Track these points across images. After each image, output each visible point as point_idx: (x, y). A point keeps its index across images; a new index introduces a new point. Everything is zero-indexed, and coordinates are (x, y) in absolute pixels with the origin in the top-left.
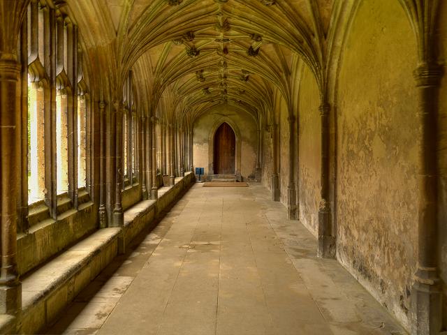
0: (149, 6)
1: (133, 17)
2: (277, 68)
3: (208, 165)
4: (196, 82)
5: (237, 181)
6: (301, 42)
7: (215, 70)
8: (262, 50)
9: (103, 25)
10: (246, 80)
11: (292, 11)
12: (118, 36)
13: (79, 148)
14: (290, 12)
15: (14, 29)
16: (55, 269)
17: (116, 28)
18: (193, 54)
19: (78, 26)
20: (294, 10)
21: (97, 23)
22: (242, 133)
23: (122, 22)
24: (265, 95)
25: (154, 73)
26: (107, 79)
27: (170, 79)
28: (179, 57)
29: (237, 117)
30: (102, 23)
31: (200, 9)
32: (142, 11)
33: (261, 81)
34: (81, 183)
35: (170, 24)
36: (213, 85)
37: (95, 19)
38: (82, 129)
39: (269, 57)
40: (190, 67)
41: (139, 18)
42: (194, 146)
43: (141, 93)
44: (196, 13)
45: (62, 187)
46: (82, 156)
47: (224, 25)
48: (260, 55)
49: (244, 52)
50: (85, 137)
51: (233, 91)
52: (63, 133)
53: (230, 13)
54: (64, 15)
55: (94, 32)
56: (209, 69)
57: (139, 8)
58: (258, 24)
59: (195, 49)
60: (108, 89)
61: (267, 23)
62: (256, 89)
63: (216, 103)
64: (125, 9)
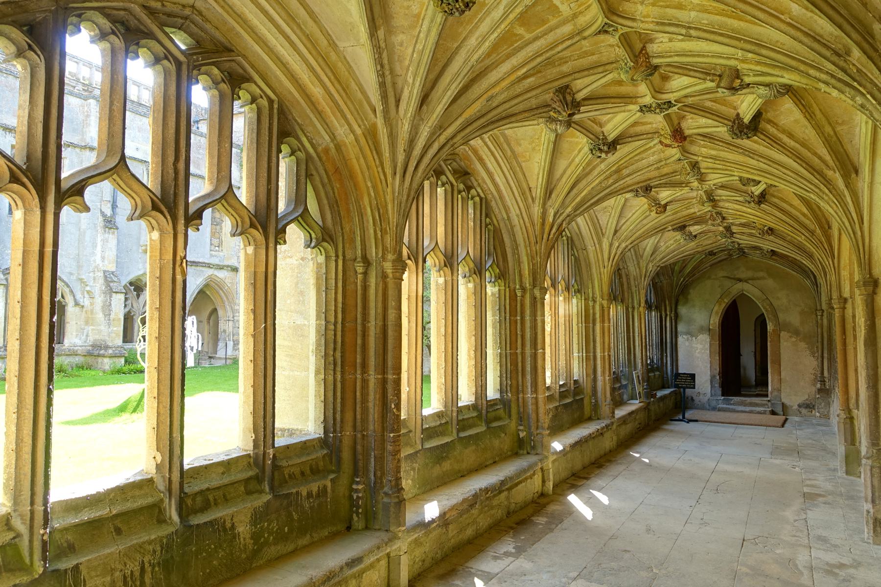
3: (708, 378)
5: (773, 413)
6: (840, 55)
8: (769, 122)
10: (759, 203)
16: (862, 363)
22: (781, 316)
24: (812, 233)
33: (796, 202)
34: (492, 393)
36: (699, 220)
39: (791, 136)
42: (681, 340)
49: (722, 131)
53: (634, 20)
55: (320, 114)
58: (734, 37)
61: (735, 23)
62: (788, 220)
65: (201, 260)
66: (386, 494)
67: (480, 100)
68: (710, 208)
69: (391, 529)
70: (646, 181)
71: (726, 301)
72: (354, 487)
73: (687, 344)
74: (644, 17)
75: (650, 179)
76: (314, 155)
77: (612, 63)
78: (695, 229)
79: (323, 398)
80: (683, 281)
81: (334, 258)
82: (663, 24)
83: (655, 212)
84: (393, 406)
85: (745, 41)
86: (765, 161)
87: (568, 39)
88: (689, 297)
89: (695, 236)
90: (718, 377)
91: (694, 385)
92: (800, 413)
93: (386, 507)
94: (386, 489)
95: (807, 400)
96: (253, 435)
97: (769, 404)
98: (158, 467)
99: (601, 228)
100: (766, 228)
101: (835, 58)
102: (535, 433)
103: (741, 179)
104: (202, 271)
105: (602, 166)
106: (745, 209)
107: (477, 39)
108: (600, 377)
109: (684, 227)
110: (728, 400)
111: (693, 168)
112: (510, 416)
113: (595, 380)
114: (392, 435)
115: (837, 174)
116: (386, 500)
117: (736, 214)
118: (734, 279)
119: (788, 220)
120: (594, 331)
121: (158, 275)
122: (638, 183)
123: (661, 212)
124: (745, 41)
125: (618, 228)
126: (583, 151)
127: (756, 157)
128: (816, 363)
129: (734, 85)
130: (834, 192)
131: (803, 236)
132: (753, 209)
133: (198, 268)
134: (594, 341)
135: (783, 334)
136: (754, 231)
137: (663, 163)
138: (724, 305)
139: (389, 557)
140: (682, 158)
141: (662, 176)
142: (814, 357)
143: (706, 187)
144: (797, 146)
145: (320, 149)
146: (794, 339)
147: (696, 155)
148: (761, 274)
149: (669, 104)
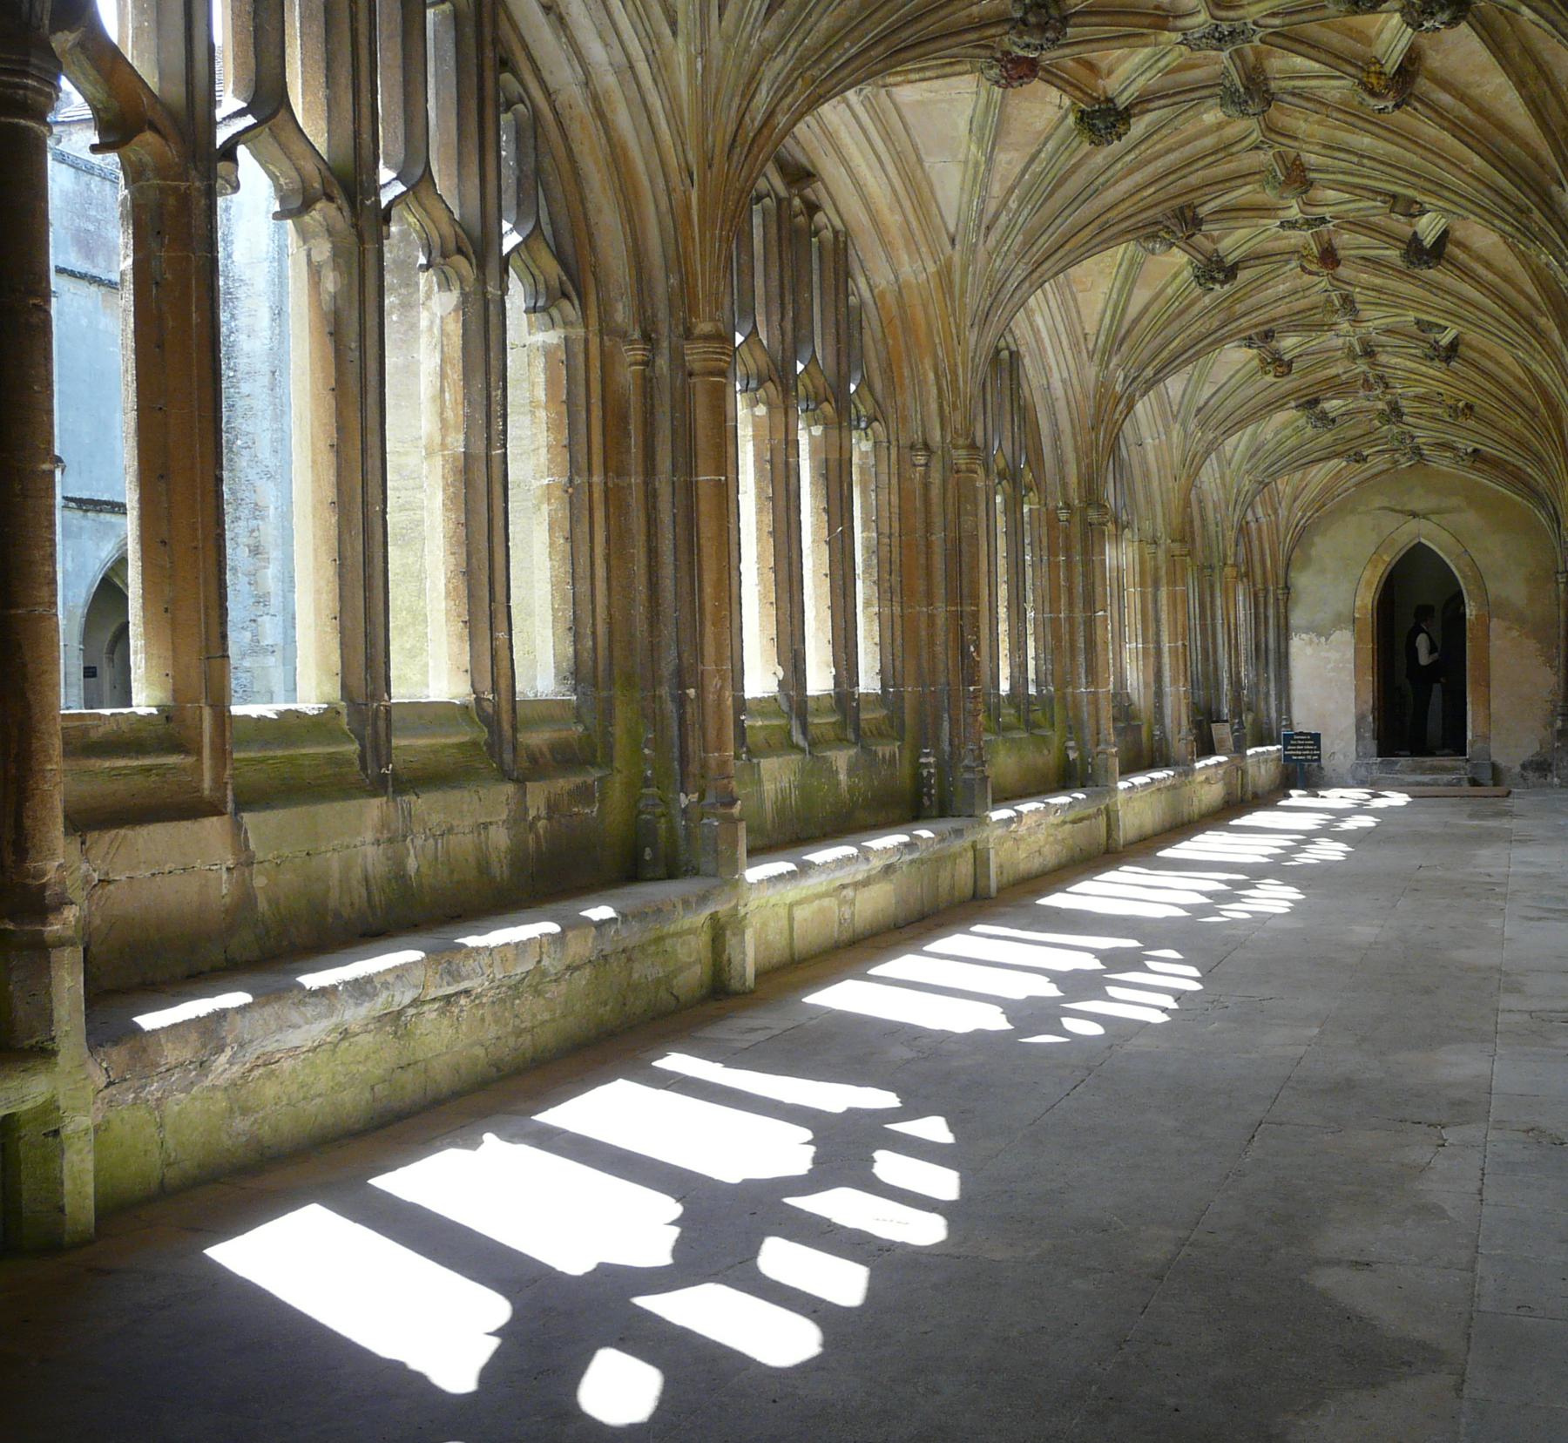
0: (1039, 151)
1: (997, 189)
2: (1523, 303)
5: (1474, 782)
7: (1321, 327)
8: (1460, 244)
9: (914, 224)
10: (1447, 360)
11: (1471, 115)
12: (958, 247)
13: (859, 584)
14: (1465, 120)
15: (718, 269)
17: (952, 229)
18: (1214, 280)
19: (847, 234)
20: (1480, 110)
21: (898, 218)
23: (964, 207)
24: (1533, 412)
25: (1091, 356)
26: (931, 375)
27: (1149, 372)
28: (1169, 291)
29: (1470, 519)
30: (912, 218)
31: (1197, 137)
32: (1018, 170)
34: (868, 682)
35: (1110, 195)
36: (1339, 387)
37: (891, 210)
38: (865, 528)
39: (1488, 265)
40: (1216, 324)
41: (1011, 190)
43: (1055, 424)
44: (1187, 150)
45: (819, 680)
46: (867, 604)
47: (1288, 176)
48: (1453, 262)
49: (1393, 254)
50: (873, 550)
51: (1427, 410)
53: (1296, 138)
54: (812, 208)
55: (886, 245)
56: (1294, 328)
57: (1009, 163)
59: (1221, 260)
60: (934, 407)
62: (1494, 389)
63: (1378, 463)
64: (971, 171)
65: (105, 498)
66: (968, 769)
67: (1091, 227)
68: (1365, 368)
69: (977, 813)
70: (1268, 322)
71: (1387, 559)
72: (923, 760)
73: (1309, 651)
74: (1308, 136)
75: (1274, 320)
76: (871, 302)
77: (1255, 173)
78: (1333, 405)
79: (877, 640)
80: (1302, 518)
81: (885, 444)
82: (1330, 147)
83: (1272, 374)
84: (972, 649)
85: (1425, 179)
86: (1455, 300)
87: (1212, 154)
88: (1313, 552)
89: (1333, 421)
90: (1371, 718)
91: (1319, 755)
93: (969, 785)
94: (966, 762)
95: (1538, 754)
96: (833, 670)
98: (780, 683)
99: (1170, 403)
100: (1461, 405)
101: (1517, 215)
102: (1094, 751)
103: (1418, 322)
104: (112, 526)
105: (1207, 300)
106: (1424, 369)
107: (1104, 158)
108: (1168, 689)
109: (1316, 401)
111: (1344, 302)
112: (1053, 725)
113: (1159, 694)
114: (971, 688)
115: (1552, 324)
116: (967, 776)
117: (1409, 379)
118: (1401, 512)
119: (1494, 389)
120: (1156, 601)
121: (768, 458)
122: (1256, 326)
123: (1283, 375)
124: (1425, 179)
126: (1180, 278)
127: (1440, 293)
128: (1555, 679)
129: (1412, 211)
130: (1549, 350)
131: (1519, 420)
132: (1439, 369)
133: (102, 515)
134: (1157, 620)
135: (1495, 623)
136: (1439, 411)
137: (1298, 296)
138: (1381, 569)
139: (975, 851)
140: (1330, 288)
141: (1294, 314)
142: (1551, 667)
143: (1362, 330)
144: (1498, 280)
145: (876, 291)
146: (1515, 634)
147: (1349, 284)
148: (1454, 501)
149: (1323, 220)
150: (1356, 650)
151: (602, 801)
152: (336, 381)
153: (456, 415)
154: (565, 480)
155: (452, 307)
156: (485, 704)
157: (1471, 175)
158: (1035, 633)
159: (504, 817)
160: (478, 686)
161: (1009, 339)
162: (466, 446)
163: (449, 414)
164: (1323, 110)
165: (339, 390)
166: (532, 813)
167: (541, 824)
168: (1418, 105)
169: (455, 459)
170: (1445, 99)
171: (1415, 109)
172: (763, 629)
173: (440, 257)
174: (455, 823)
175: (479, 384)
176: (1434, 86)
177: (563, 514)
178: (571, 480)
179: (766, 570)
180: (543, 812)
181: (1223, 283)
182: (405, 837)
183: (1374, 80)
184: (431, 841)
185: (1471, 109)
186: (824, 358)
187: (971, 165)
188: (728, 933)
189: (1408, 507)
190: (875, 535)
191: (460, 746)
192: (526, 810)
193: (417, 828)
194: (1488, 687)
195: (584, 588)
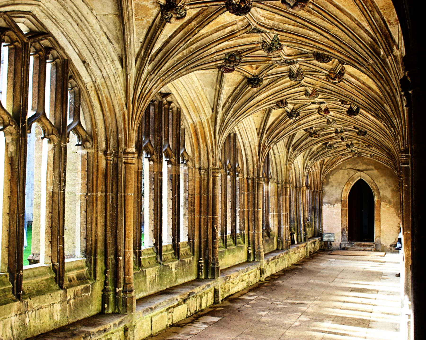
0: (237, 87)
4: (310, 138)
18: (293, 116)
19: (180, 109)
28: (281, 118)
32: (231, 91)
41: (229, 97)
44: (282, 86)
52: (168, 196)
72: (200, 261)
73: (328, 209)
79: (187, 225)
92: (391, 250)
97: (374, 245)
98: (154, 244)
110: (351, 244)
124: (350, 99)
125: (215, 67)
135: (382, 203)
137: (319, 119)
146: (388, 206)
148: (371, 167)
150: (342, 210)
151: (92, 291)
152: (11, 177)
153: (50, 180)
154: (85, 194)
155: (51, 149)
156: (55, 266)
157: (362, 100)
158: (240, 215)
159: (59, 301)
160: (53, 261)
161: (233, 130)
162: (53, 190)
163: (49, 180)
164: (319, 80)
165: (11, 180)
166: (68, 298)
167: (72, 301)
168: (345, 82)
169: (50, 193)
170: (353, 80)
171: (344, 83)
172: (150, 228)
173: (47, 134)
174: (42, 305)
175: (57, 171)
176: (350, 77)
177: (84, 204)
178: (87, 194)
179: (151, 210)
180: (72, 297)
181: (295, 117)
182: (25, 312)
183: (332, 75)
184: (34, 312)
185: (362, 83)
186: (172, 145)
187: (217, 91)
188: (129, 330)
189: (357, 168)
190: (187, 194)
191: (47, 280)
192: (66, 297)
193: (29, 309)
194: (380, 222)
195: (89, 226)
